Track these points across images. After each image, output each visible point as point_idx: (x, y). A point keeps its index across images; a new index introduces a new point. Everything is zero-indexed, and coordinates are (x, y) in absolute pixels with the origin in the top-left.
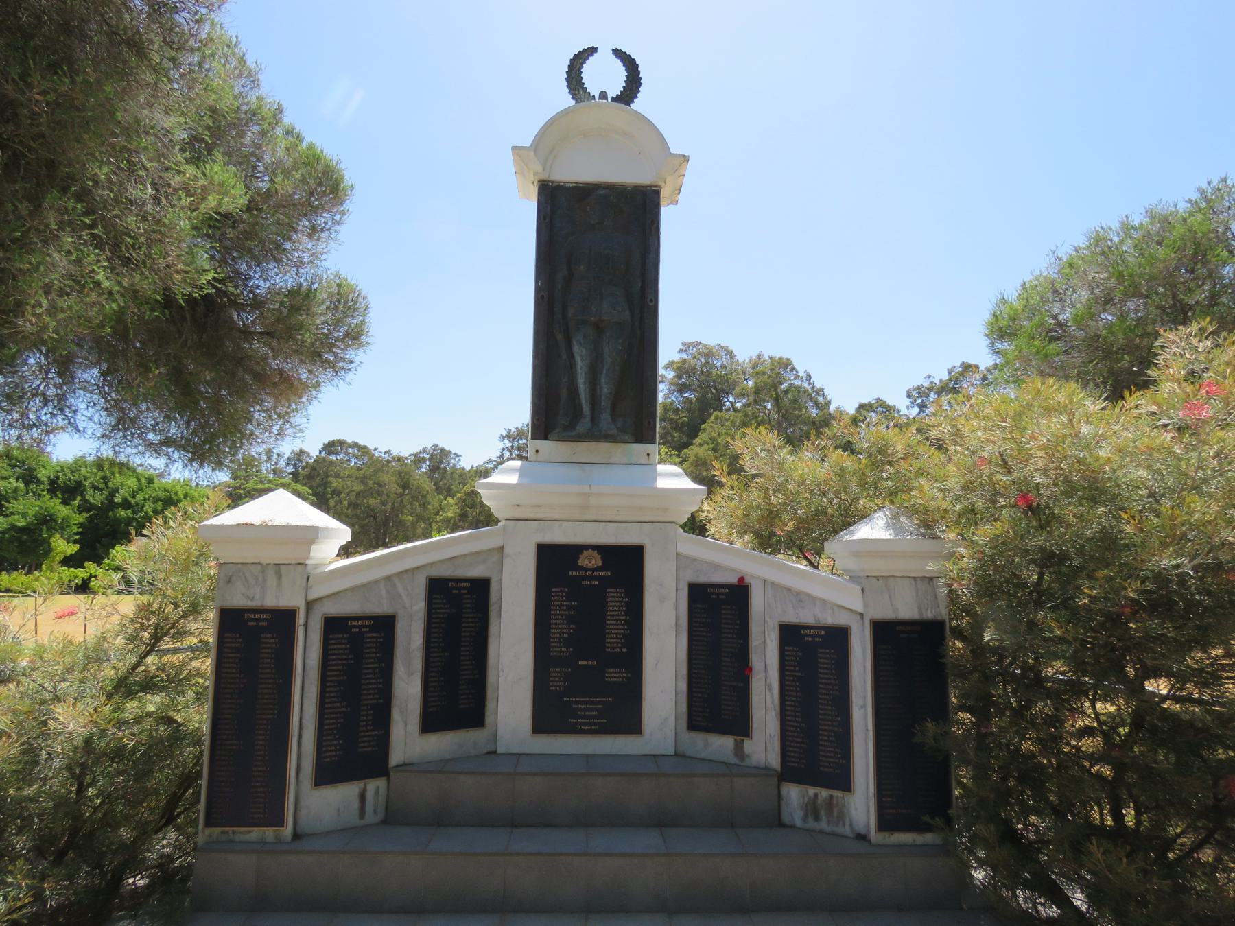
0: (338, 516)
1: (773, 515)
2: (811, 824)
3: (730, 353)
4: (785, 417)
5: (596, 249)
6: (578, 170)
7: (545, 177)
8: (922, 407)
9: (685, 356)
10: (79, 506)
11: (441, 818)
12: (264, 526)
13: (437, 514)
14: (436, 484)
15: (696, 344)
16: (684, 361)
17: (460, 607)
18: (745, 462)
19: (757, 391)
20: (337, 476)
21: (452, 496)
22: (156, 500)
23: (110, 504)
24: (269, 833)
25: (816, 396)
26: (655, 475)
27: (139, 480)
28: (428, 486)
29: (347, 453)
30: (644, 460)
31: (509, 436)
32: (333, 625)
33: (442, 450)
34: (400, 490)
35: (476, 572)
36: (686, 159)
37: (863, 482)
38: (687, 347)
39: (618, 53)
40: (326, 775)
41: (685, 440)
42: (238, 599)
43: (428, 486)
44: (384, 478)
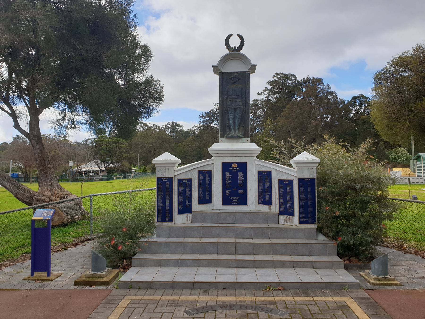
2: (286, 223)
9: (275, 79)
17: (205, 177)
39: (238, 35)
40: (180, 212)
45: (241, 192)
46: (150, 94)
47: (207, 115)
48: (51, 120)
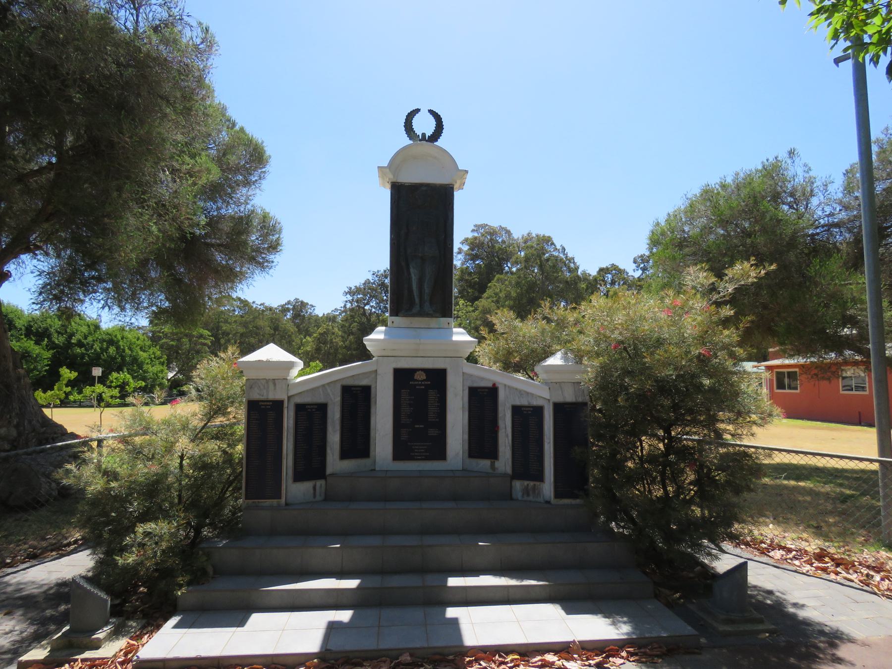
0: (301, 359)
1: (509, 353)
2: (526, 498)
3: (508, 232)
4: (547, 278)
5: (420, 210)
6: (410, 177)
7: (394, 180)
8: (644, 269)
9: (476, 235)
10: (47, 346)
11: (351, 498)
12: (268, 362)
13: (299, 348)
14: (298, 327)
15: (483, 226)
16: (475, 238)
17: (357, 398)
18: (498, 327)
19: (527, 259)
20: (226, 322)
21: (310, 336)
22: (103, 341)
23: (68, 345)
24: (275, 502)
25: (568, 263)
26: (451, 334)
27: (89, 326)
28: (292, 328)
29: (232, 305)
30: (447, 326)
31: (350, 292)
32: (300, 408)
33: (302, 302)
34: (272, 332)
35: (364, 382)
36: (467, 172)
37: (553, 337)
38: (477, 228)
40: (298, 477)
41: (477, 294)
42: (256, 396)
43: (292, 328)
44: (261, 323)
45: (433, 432)
46: (248, 243)
47: (358, 290)
48: (850, 645)
